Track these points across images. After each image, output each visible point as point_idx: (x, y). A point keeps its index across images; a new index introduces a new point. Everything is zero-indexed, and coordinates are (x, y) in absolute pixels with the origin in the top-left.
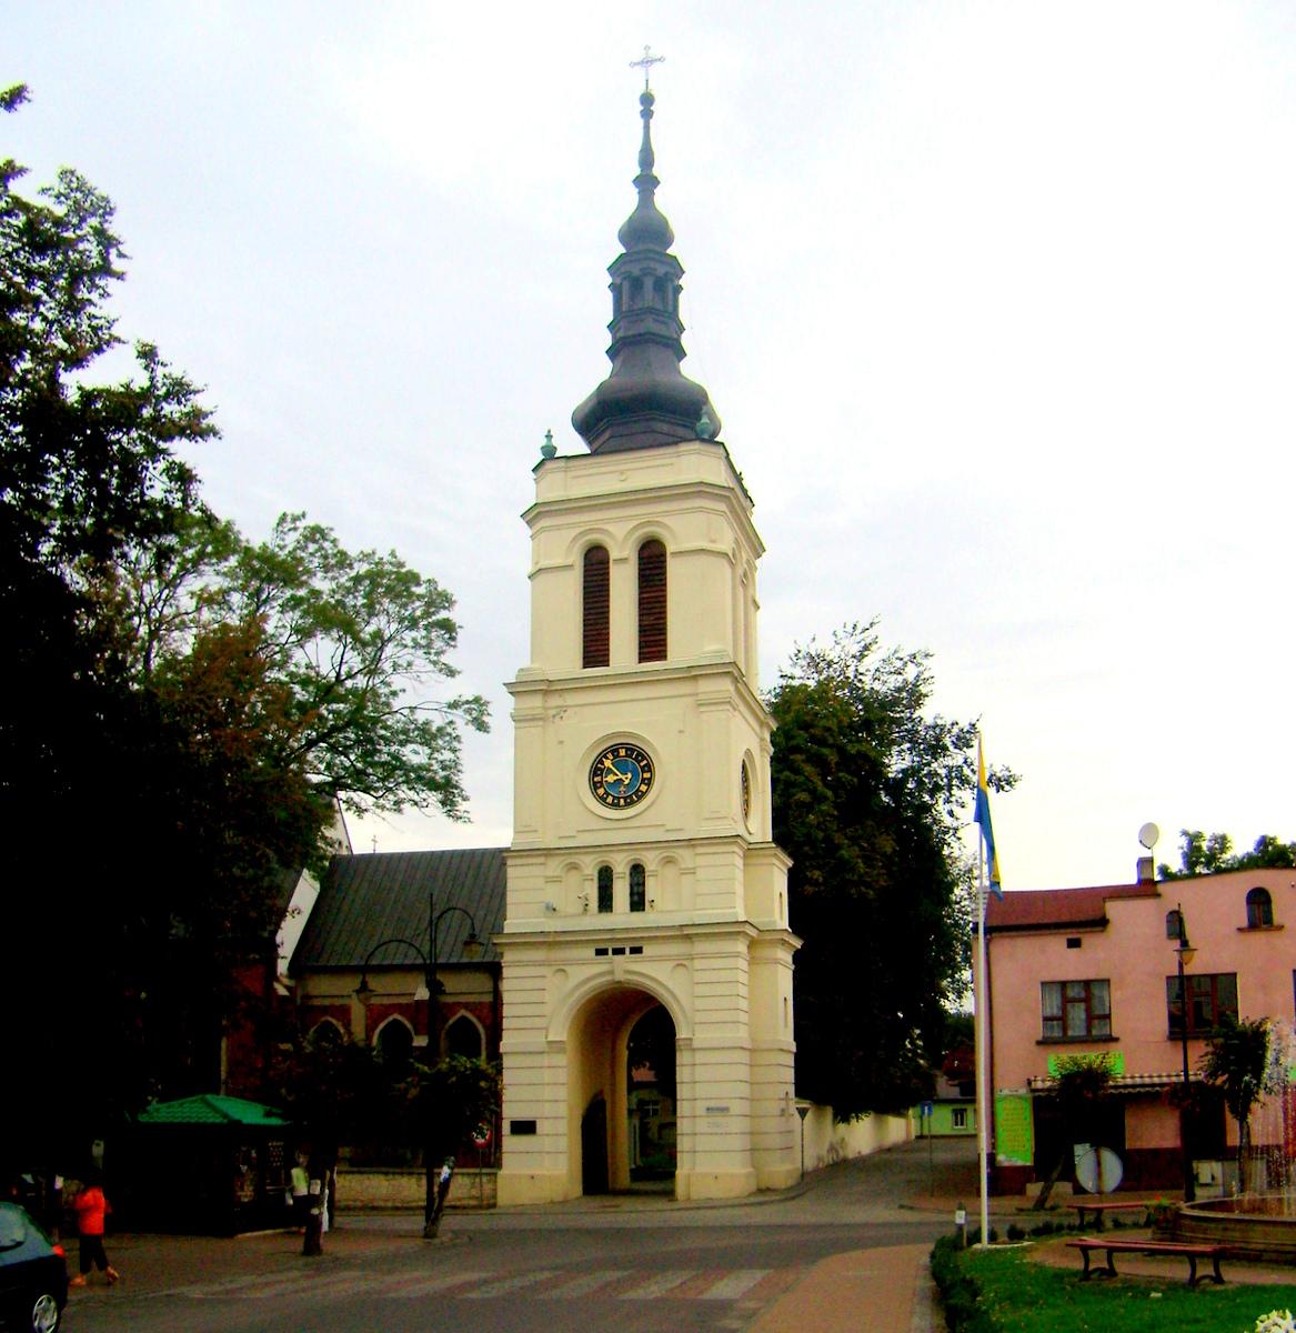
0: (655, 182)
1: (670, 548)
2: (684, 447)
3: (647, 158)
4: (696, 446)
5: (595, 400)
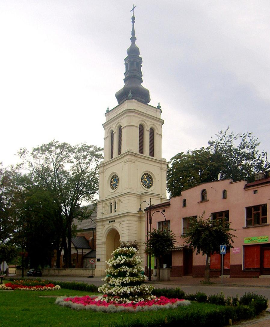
0: (135, 39)
3: (133, 33)
5: (123, 90)
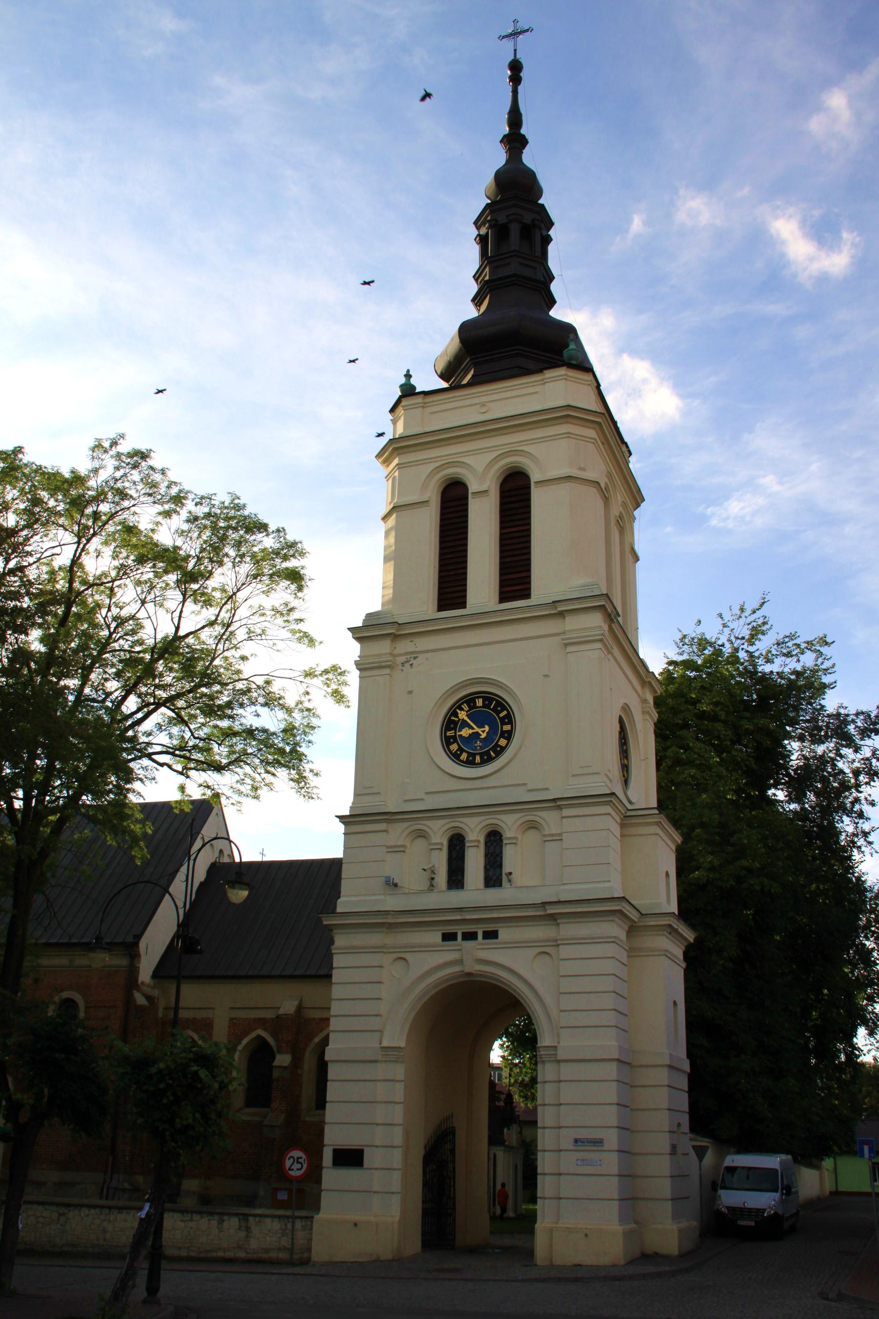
1: (535, 476)
2: (549, 374)
3: (515, 118)
4: (562, 371)
